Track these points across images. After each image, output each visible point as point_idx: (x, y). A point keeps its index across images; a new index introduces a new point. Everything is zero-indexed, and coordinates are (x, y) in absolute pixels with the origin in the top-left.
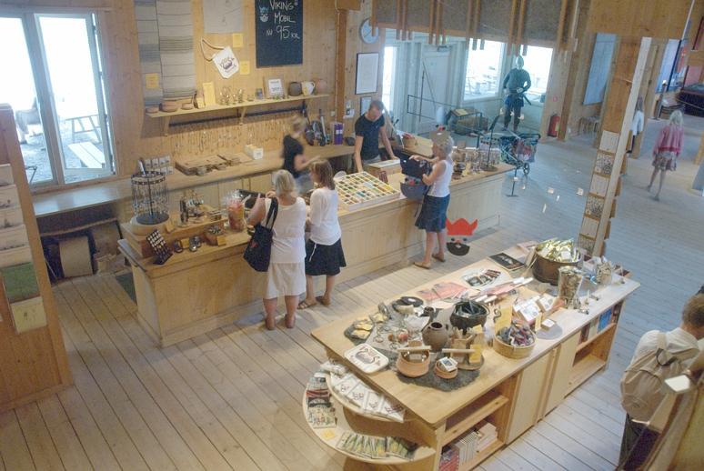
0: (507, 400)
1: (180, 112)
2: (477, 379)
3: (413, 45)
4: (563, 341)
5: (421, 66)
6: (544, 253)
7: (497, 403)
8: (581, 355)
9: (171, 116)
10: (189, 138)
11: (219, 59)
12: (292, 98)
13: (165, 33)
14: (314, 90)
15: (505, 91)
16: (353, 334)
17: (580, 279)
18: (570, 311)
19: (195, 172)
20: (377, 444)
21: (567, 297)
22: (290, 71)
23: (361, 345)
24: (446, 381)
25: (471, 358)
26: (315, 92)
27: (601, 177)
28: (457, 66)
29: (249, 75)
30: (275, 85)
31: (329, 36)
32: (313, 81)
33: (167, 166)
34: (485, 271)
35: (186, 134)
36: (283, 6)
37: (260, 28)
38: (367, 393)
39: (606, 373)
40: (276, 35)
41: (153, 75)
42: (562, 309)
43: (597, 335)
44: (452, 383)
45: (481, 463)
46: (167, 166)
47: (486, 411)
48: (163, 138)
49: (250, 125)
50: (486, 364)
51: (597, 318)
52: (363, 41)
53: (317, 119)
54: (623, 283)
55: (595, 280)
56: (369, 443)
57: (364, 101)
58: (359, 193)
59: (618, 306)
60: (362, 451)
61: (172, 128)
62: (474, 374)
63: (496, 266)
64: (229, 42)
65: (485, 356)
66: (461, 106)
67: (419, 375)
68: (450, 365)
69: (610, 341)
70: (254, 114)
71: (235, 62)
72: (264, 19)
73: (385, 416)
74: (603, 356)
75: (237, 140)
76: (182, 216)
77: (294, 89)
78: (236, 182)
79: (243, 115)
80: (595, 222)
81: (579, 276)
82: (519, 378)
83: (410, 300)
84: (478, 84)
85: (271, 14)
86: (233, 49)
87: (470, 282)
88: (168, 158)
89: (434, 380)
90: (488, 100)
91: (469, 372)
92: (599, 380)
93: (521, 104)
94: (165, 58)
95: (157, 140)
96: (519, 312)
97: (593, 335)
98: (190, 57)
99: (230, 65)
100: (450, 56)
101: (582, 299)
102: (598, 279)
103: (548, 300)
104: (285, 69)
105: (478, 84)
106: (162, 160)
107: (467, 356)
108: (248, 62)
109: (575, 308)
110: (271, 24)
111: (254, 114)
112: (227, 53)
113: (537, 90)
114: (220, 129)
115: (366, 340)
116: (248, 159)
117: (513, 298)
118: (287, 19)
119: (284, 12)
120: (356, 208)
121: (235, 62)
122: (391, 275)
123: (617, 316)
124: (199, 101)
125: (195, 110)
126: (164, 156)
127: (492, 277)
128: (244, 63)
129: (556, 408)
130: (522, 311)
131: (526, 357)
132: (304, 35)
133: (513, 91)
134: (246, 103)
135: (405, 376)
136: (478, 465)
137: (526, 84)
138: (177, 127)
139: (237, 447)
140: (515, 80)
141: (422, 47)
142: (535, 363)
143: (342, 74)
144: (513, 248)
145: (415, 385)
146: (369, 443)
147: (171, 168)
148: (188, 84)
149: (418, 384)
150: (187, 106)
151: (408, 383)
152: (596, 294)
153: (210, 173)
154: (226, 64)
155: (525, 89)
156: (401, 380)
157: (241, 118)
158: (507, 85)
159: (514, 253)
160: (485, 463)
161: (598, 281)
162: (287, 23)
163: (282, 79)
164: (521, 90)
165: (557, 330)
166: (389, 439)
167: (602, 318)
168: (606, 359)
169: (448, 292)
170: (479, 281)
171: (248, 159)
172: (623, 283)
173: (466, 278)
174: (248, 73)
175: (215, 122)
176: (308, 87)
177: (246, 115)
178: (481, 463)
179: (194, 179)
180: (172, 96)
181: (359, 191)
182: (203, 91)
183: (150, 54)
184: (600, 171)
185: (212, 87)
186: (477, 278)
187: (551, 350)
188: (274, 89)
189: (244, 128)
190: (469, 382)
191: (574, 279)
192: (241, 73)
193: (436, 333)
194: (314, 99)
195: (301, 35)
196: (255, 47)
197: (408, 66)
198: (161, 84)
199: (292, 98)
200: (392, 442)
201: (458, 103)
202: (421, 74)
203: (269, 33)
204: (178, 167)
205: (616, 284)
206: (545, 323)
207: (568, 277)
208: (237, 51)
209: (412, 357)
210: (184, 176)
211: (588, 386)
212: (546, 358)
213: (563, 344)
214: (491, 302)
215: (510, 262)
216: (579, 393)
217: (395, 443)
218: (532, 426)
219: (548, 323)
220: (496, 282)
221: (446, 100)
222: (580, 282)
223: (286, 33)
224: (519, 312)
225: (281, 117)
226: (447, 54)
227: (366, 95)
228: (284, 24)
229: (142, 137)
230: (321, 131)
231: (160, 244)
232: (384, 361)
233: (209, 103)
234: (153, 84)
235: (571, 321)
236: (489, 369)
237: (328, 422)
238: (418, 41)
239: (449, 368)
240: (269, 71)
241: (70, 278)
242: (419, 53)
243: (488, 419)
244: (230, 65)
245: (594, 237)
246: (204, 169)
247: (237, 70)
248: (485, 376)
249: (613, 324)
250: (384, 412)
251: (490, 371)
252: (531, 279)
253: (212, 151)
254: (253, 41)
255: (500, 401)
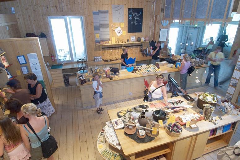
0: (170, 151)
1: (105, 44)
3: (185, 27)
5: (187, 33)
7: (165, 151)
8: (210, 141)
9: (102, 46)
10: (107, 52)
11: (117, 30)
12: (137, 42)
13: (102, 23)
15: (218, 42)
17: (212, 110)
18: (207, 122)
19: (107, 61)
20: (112, 155)
21: (207, 116)
24: (139, 139)
26: (145, 41)
27: (238, 71)
28: (201, 35)
30: (133, 38)
31: (151, 24)
32: (145, 37)
33: (100, 59)
35: (107, 51)
37: (129, 21)
40: (134, 23)
41: (97, 34)
43: (221, 134)
45: (209, 153)
46: (100, 59)
50: (160, 136)
51: (221, 127)
52: (162, 25)
53: (146, 49)
54: (238, 115)
55: (224, 111)
56: (110, 154)
58: (148, 71)
59: (234, 124)
60: (106, 157)
61: (103, 49)
63: (183, 99)
64: (120, 25)
65: (160, 132)
69: (230, 137)
71: (121, 31)
72: (131, 18)
73: (115, 146)
74: (227, 142)
76: (91, 72)
77: (139, 39)
78: (118, 65)
80: (234, 89)
81: (212, 109)
82: (174, 144)
83: (144, 106)
85: (133, 17)
86: (121, 28)
88: (101, 57)
89: (135, 137)
91: (149, 138)
94: (101, 30)
95: (98, 52)
96: (181, 118)
98: (108, 30)
99: (120, 32)
100: (198, 31)
101: (214, 118)
102: (226, 112)
103: (197, 116)
106: (97, 57)
107: (151, 131)
108: (125, 32)
109: (210, 121)
110: (133, 20)
112: (119, 29)
114: (116, 50)
115: (122, 117)
117: (183, 112)
118: (137, 18)
119: (137, 16)
120: (145, 75)
121: (121, 31)
123: (234, 128)
124: (110, 42)
125: (109, 44)
127: (179, 103)
128: (124, 31)
129: (199, 158)
130: (182, 118)
131: (177, 137)
132: (143, 23)
133: (221, 42)
134: (124, 43)
135: (126, 133)
136: (207, 154)
137: (226, 39)
138: (104, 49)
139: (85, 142)
141: (188, 28)
144: (193, 94)
145: (128, 137)
146: (110, 154)
147: (101, 60)
148: (107, 37)
149: (130, 137)
151: (126, 136)
152: (222, 117)
153: (111, 62)
154: (119, 32)
155: (226, 41)
156: (125, 135)
159: (192, 96)
160: (210, 154)
162: (138, 20)
165: (197, 129)
166: (118, 154)
167: (224, 127)
169: (159, 106)
170: (177, 103)
172: (238, 115)
174: (125, 34)
176: (143, 39)
178: (209, 153)
180: (102, 40)
181: (148, 70)
182: (111, 39)
183: (97, 28)
184: (237, 69)
185: (114, 38)
187: (192, 136)
188: (132, 39)
190: (148, 142)
192: (123, 34)
193: (142, 120)
194: (145, 43)
195: (142, 23)
196: (127, 27)
197: (182, 33)
199: (137, 42)
200: (118, 156)
201: (200, 46)
202: (187, 36)
203: (132, 23)
205: (234, 115)
207: (207, 109)
208: (122, 28)
210: (104, 62)
212: (189, 139)
214: (172, 112)
215: (190, 99)
217: (119, 157)
219: (193, 126)
221: (196, 45)
222: (213, 112)
223: (137, 23)
224: (181, 118)
225: (130, 48)
226: (197, 30)
228: (136, 20)
229: (94, 51)
230: (147, 52)
231: (82, 79)
233: (113, 42)
234: (98, 36)
235: (206, 126)
236: (160, 138)
237: (103, 142)
238: (187, 26)
239: (141, 134)
240: (131, 34)
241: (72, 85)
242: (187, 30)
244: (120, 32)
245: (233, 94)
246: (109, 61)
248: (156, 141)
249: (231, 131)
255: (167, 151)
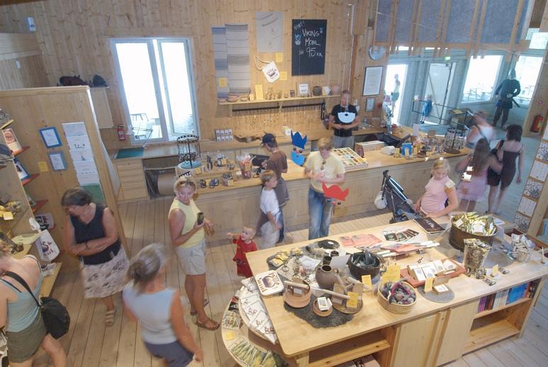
0: (388, 346)
1: (239, 102)
2: (348, 324)
3: (421, 62)
4: (455, 306)
6: (459, 224)
8: (479, 323)
10: (244, 119)
11: (266, 70)
12: (314, 97)
13: (232, 52)
14: (331, 92)
15: (497, 96)
16: (271, 261)
17: (484, 253)
18: (472, 279)
19: (244, 140)
20: (257, 355)
21: (472, 266)
22: (313, 78)
23: (272, 271)
24: (318, 318)
25: (347, 303)
26: (331, 93)
29: (287, 81)
30: (303, 87)
32: (331, 86)
34: (405, 230)
36: (312, 33)
37: (295, 49)
38: (259, 310)
39: (519, 341)
42: (463, 276)
43: (505, 306)
44: (322, 321)
47: (361, 352)
48: (230, 119)
49: (286, 114)
50: (365, 311)
54: (543, 263)
55: (511, 255)
57: (369, 101)
60: (242, 358)
61: (234, 113)
62: (345, 318)
64: (273, 59)
66: (458, 108)
67: (303, 306)
68: (324, 305)
69: (524, 313)
70: (288, 107)
71: (277, 72)
72: (298, 43)
73: (263, 334)
74: (518, 324)
75: (277, 122)
77: (317, 91)
79: (281, 107)
80: (533, 203)
81: (484, 250)
82: (398, 329)
84: (484, 93)
85: (303, 40)
86: (276, 64)
87: (387, 238)
89: (308, 314)
90: (483, 104)
91: (341, 315)
92: (509, 346)
93: (511, 106)
95: (225, 119)
96: (413, 270)
97: (499, 305)
98: (247, 68)
99: (274, 74)
101: (488, 271)
104: (311, 78)
105: (484, 93)
106: (222, 132)
107: (345, 301)
108: (286, 73)
109: (478, 278)
111: (288, 107)
113: (526, 96)
115: (277, 268)
116: (283, 135)
117: (419, 257)
118: (314, 42)
119: (312, 38)
121: (277, 72)
122: (357, 220)
123: (533, 293)
124: (251, 96)
125: (248, 102)
126: (228, 129)
129: (454, 361)
130: (416, 271)
133: (504, 96)
134: (283, 99)
135: (289, 306)
136: (473, 352)
138: (238, 112)
140: (508, 87)
142: (417, 321)
143: (355, 81)
147: (232, 137)
148: (246, 85)
150: (243, 99)
151: (289, 311)
152: (506, 269)
153: (254, 142)
157: (280, 109)
158: (500, 92)
161: (504, 258)
162: (314, 46)
163: (309, 86)
164: (510, 95)
166: (269, 353)
168: (520, 328)
171: (283, 135)
173: (385, 233)
174: (286, 79)
175: (263, 110)
177: (283, 107)
179: (244, 144)
182: (254, 90)
183: (221, 65)
184: (541, 158)
185: (261, 89)
186: (394, 235)
187: (437, 312)
189: (281, 114)
190: (338, 325)
191: (478, 252)
192: (281, 79)
195: (324, 55)
198: (228, 84)
199: (314, 97)
203: (302, 53)
204: (237, 138)
206: (438, 288)
209: (296, 291)
211: (495, 349)
213: (453, 311)
216: (483, 354)
217: (272, 359)
218: (454, 361)
220: (411, 241)
222: (485, 256)
224: (413, 270)
227: (370, 97)
228: (312, 46)
232: (280, 288)
233: (259, 97)
234: (223, 84)
235: (469, 288)
236: (364, 317)
237: (234, 326)
238: (426, 59)
239: (321, 307)
240: (300, 78)
241: (164, 196)
243: (375, 356)
244: (274, 74)
245: (530, 216)
247: (278, 77)
248: (357, 323)
250: (263, 331)
251: (365, 318)
252: (438, 244)
253: (261, 128)
254: (290, 57)
255: (382, 345)
